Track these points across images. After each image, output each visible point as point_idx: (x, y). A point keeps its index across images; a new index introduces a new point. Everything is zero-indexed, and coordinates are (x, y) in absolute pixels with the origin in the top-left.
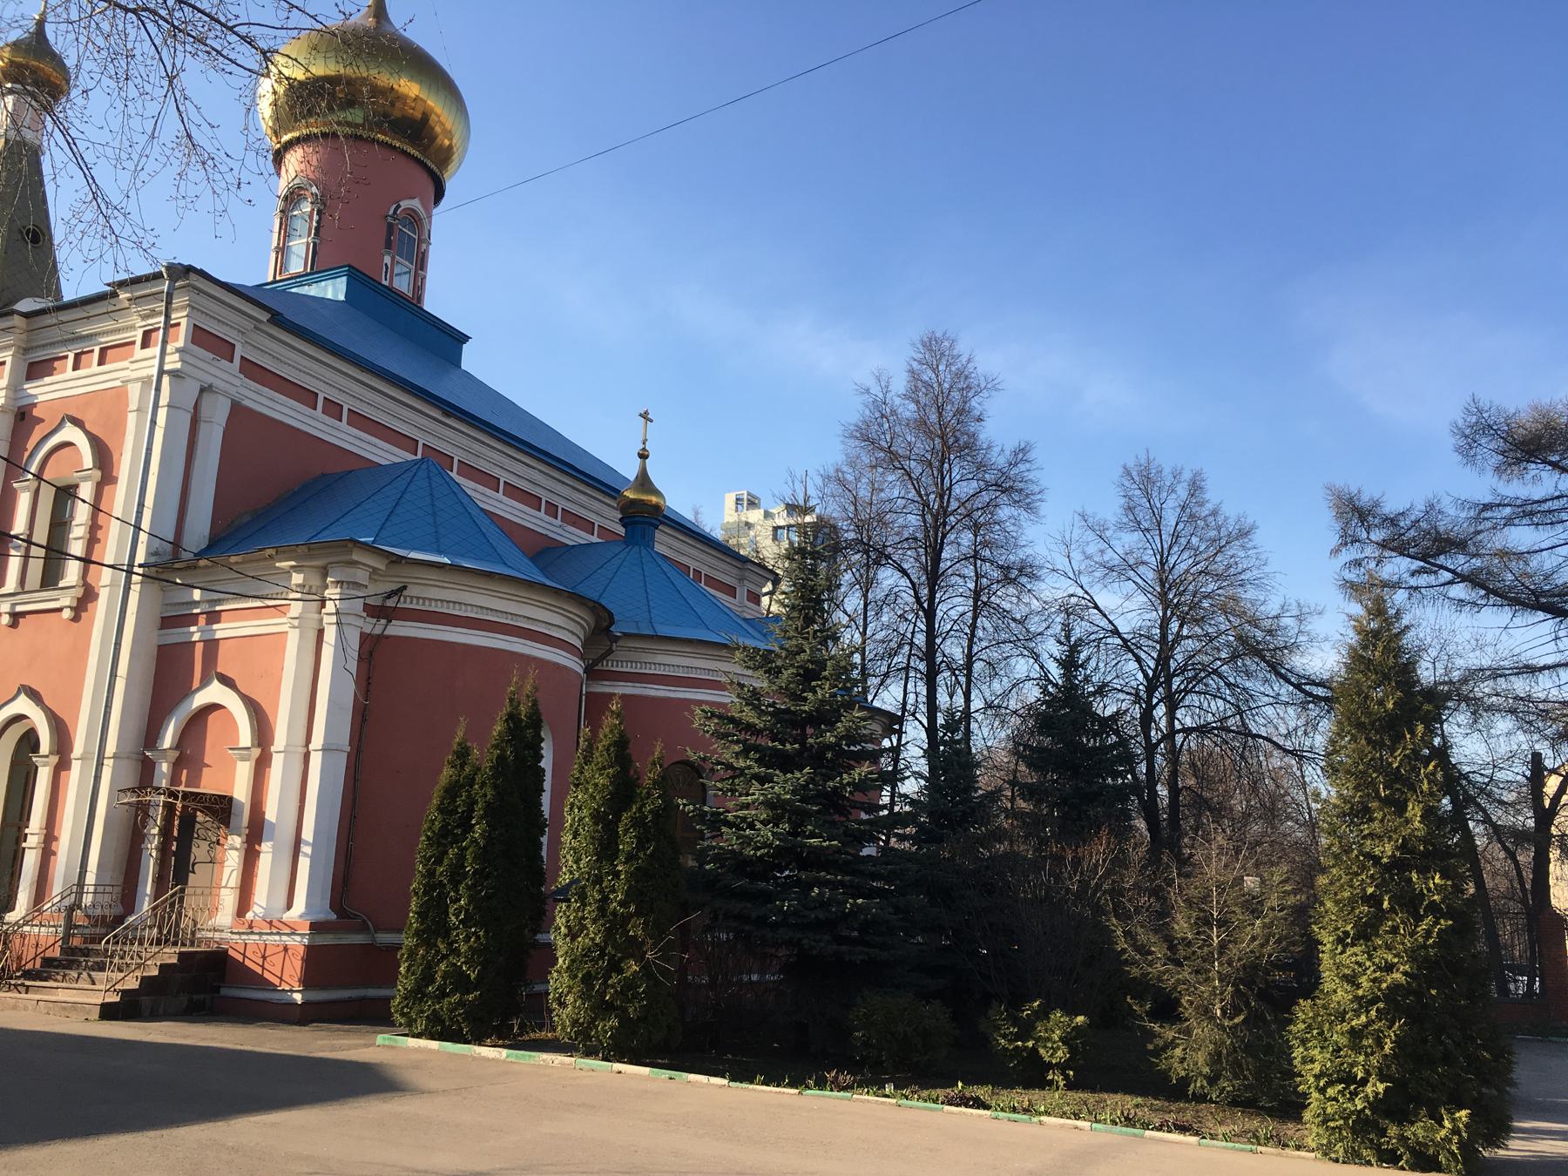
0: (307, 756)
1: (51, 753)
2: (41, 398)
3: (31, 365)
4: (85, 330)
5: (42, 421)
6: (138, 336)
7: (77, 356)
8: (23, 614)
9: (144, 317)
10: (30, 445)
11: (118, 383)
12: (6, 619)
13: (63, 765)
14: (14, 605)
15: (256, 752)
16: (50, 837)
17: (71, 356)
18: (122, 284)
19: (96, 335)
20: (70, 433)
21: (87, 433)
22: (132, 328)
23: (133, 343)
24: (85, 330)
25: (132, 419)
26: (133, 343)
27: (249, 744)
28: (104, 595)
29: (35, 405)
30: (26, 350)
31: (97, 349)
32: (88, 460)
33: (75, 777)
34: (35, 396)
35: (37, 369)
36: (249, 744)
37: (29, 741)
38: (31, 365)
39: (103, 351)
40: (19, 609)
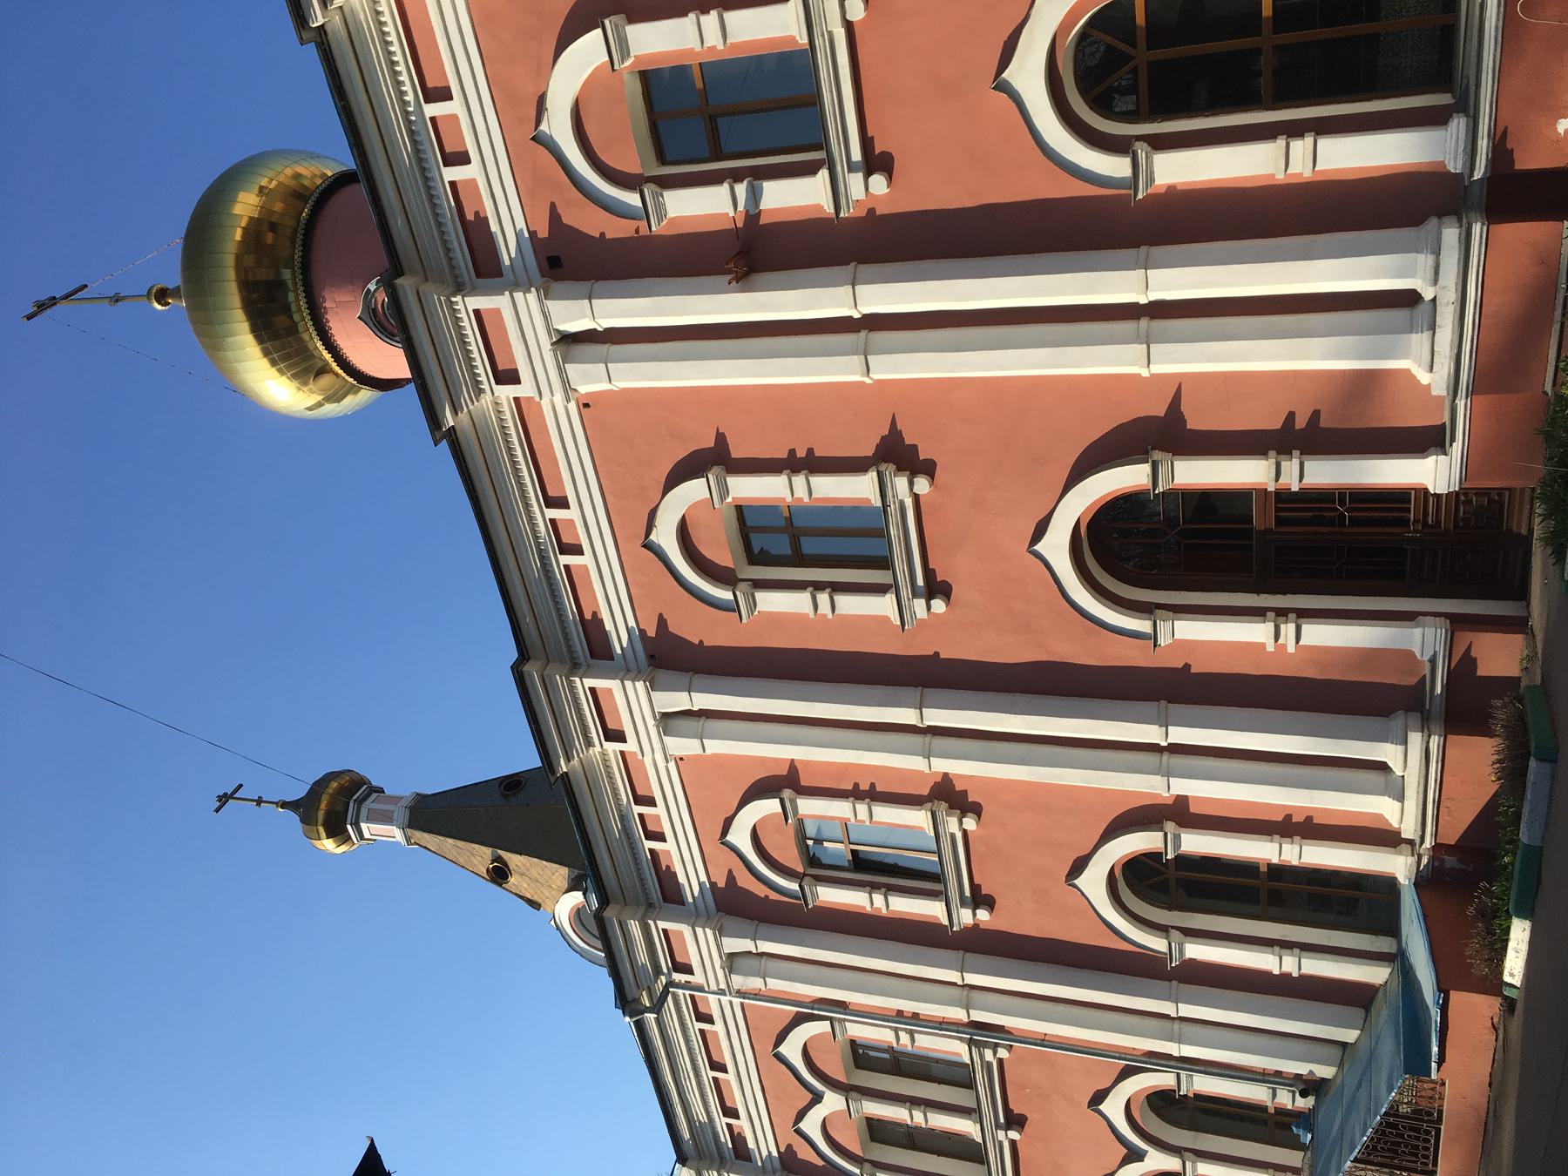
1: (1161, 830)
2: (521, 224)
4: (615, 826)
6: (612, 748)
7: (650, 836)
9: (589, 743)
10: (760, 890)
11: (672, 765)
12: (938, 605)
13: (1181, 814)
14: (852, 168)
15: (1170, 826)
16: (1295, 510)
17: (565, 559)
18: (434, 420)
19: (620, 811)
20: (740, 837)
21: (743, 803)
23: (622, 753)
24: (615, 826)
25: (715, 747)
26: (622, 753)
27: (1161, 834)
28: (942, 765)
29: (532, 234)
30: (650, 905)
31: (638, 809)
32: (770, 806)
33: (1202, 790)
34: (518, 235)
35: (669, 893)
36: (1161, 834)
37: (1162, 1102)
38: (665, 900)
39: (639, 800)
40: (857, 155)
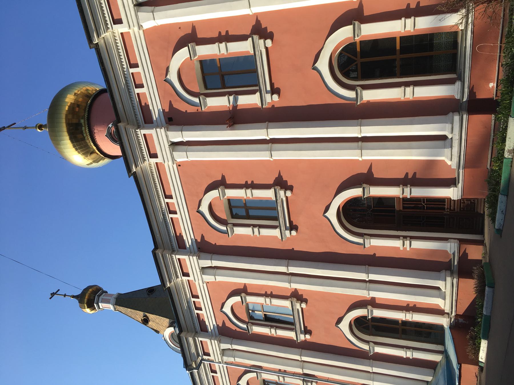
0: (371, 281)
1: (367, 308)
2: (160, 107)
3: (201, 331)
4: (185, 305)
5: (202, 235)
6: (185, 279)
7: (197, 308)
8: (291, 222)
9: (177, 277)
10: (234, 328)
12: (294, 233)
13: (373, 303)
15: (369, 307)
17: (171, 216)
19: (187, 300)
20: (227, 309)
22: (182, 281)
23: (188, 280)
24: (185, 305)
25: (219, 279)
26: (188, 280)
28: (294, 286)
29: (163, 110)
31: (193, 299)
34: (159, 111)
35: (203, 328)
36: (367, 310)
38: (201, 331)
40: (269, 88)
